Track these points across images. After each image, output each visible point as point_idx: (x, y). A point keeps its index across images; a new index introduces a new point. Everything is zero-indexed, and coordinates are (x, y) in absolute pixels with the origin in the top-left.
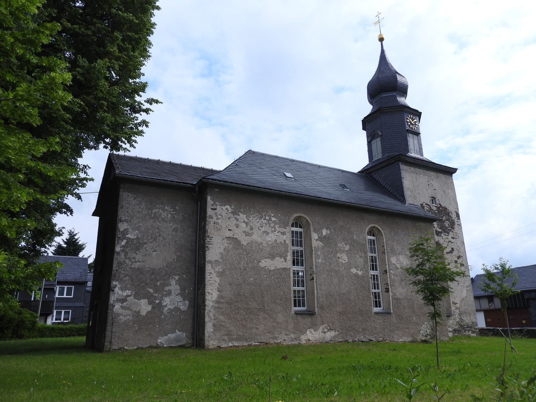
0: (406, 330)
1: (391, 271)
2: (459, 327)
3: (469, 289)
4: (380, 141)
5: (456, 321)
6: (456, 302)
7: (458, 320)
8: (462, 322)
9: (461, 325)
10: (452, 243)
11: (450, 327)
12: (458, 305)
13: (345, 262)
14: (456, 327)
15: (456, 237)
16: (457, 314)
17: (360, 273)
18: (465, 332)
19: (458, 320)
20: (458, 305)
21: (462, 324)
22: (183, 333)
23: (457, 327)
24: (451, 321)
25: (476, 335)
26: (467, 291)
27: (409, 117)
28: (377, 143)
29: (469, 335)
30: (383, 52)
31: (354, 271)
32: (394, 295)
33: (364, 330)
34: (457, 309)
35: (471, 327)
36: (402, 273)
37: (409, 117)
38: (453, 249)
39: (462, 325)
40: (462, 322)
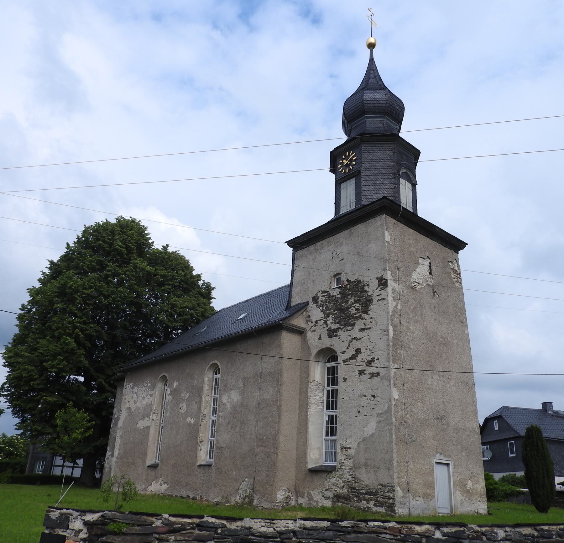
0: (223, 488)
1: (220, 414)
2: (348, 492)
3: (383, 419)
4: (355, 184)
5: (344, 480)
6: (348, 446)
7: (347, 477)
8: (355, 482)
9: (353, 489)
10: (357, 340)
11: (330, 491)
12: (351, 452)
13: (184, 411)
14: (341, 491)
15: (369, 327)
16: (347, 468)
17: (193, 421)
18: (360, 500)
19: (347, 477)
20: (351, 452)
21: (354, 485)
22: (435, 529)
23: (344, 491)
24: (333, 480)
25: (386, 510)
26: (379, 422)
27: (342, 170)
28: (349, 189)
29: (368, 508)
30: (372, 61)
31: (189, 420)
32: (217, 443)
33: (187, 484)
34: (348, 457)
35: (375, 494)
36: (231, 414)
37: (342, 170)
38: (358, 351)
39: (354, 489)
40: (355, 482)
